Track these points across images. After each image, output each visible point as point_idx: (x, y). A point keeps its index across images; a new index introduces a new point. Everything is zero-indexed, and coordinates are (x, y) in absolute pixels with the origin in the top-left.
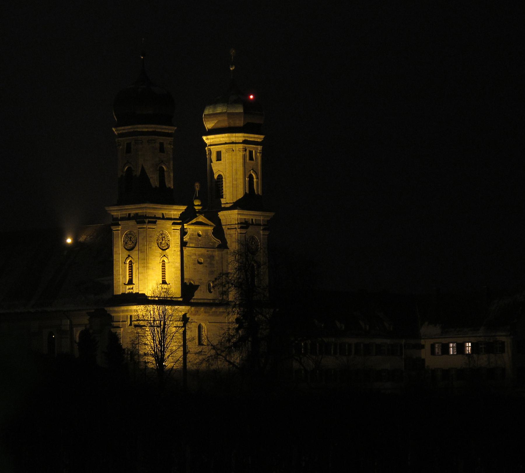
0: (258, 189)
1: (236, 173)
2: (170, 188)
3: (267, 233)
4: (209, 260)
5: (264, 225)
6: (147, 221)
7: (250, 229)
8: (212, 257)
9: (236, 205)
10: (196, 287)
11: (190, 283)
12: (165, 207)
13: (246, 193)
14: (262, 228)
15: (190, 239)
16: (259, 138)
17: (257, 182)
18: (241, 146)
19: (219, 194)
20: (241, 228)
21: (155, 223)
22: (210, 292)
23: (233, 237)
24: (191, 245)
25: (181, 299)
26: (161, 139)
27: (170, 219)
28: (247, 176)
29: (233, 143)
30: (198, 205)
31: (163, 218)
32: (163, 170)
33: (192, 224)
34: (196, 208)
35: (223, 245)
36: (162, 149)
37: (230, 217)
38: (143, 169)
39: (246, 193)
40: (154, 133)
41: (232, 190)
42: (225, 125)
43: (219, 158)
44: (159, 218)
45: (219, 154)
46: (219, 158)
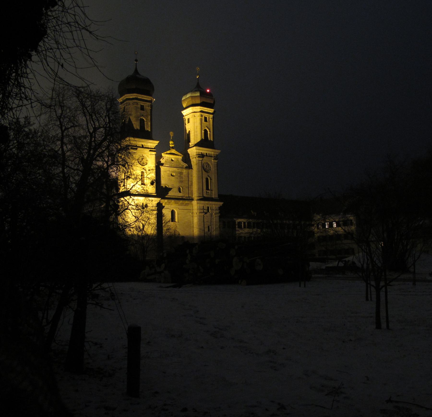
0: (210, 137)
1: (197, 128)
2: (148, 131)
3: (216, 161)
4: (179, 175)
5: (214, 157)
6: (130, 148)
7: (205, 158)
8: (181, 173)
9: (198, 145)
10: (170, 189)
11: (166, 187)
12: (143, 140)
13: (202, 139)
14: (213, 158)
15: (166, 162)
16: (211, 111)
17: (210, 134)
18: (199, 114)
19: (189, 141)
20: (199, 157)
21: (136, 149)
22: (180, 192)
23: (194, 161)
24: (166, 165)
25: (155, 194)
26: (142, 103)
27: (148, 148)
28: (203, 129)
29: (195, 112)
30: (172, 144)
31: (143, 147)
32: (144, 121)
33: (167, 154)
34: (171, 145)
35: (190, 167)
36: (142, 108)
37: (193, 151)
38: (130, 119)
39: (202, 139)
40: (136, 99)
41: (195, 136)
42: (191, 103)
43: (189, 122)
44: (140, 147)
45: (189, 119)
46: (189, 122)
